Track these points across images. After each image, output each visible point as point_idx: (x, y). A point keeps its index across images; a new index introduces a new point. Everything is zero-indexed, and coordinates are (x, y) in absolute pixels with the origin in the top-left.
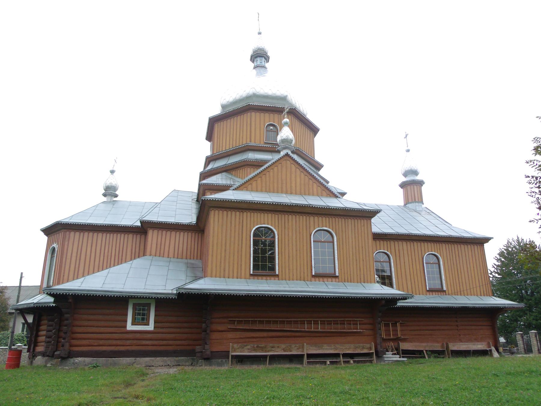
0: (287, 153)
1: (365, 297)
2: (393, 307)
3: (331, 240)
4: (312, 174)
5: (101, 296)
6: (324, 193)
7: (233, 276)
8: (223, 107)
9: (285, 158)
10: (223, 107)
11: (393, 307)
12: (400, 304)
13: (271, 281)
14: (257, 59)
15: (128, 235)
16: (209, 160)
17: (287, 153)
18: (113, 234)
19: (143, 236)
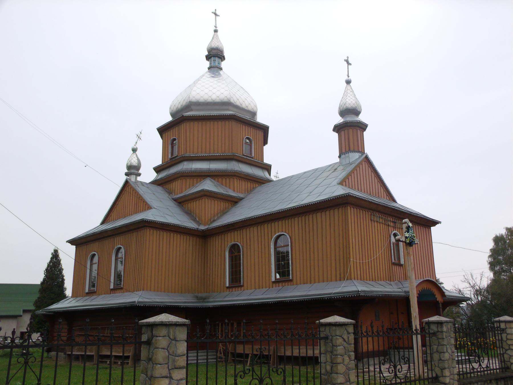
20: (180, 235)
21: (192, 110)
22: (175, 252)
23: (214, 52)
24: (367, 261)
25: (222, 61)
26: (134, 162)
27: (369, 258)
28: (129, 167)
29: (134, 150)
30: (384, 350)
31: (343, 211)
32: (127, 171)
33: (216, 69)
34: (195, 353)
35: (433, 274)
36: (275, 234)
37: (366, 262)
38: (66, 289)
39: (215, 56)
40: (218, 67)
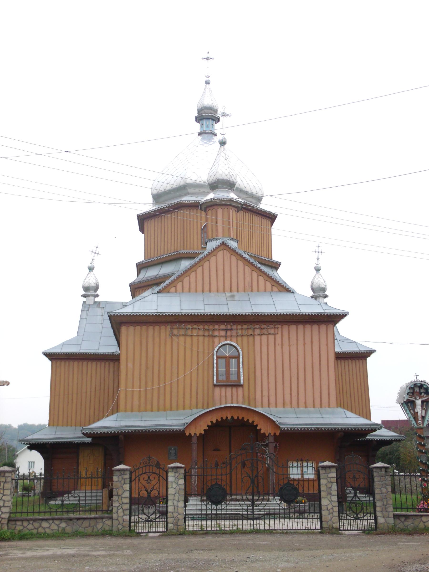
0: (223, 242)
1: (163, 429)
2: (358, 440)
3: (237, 354)
4: (172, 281)
5: (165, 431)
6: (275, 289)
7: (184, 406)
8: (157, 197)
9: (222, 248)
10: (157, 197)
11: (358, 440)
12: (369, 437)
13: (133, 413)
14: (202, 121)
15: (92, 362)
16: (141, 267)
17: (223, 242)
18: (92, 362)
19: (116, 363)
20: (96, 363)
21: (188, 194)
22: (89, 382)
23: (209, 113)
24: (156, 387)
25: (216, 123)
26: (91, 282)
27: (150, 384)
28: (86, 289)
29: (91, 269)
30: (290, 474)
31: (156, 334)
32: (83, 293)
33: (211, 135)
34: (80, 480)
35: (342, 379)
36: (219, 343)
37: (153, 389)
38: (401, 388)
39: (208, 118)
40: (211, 133)
